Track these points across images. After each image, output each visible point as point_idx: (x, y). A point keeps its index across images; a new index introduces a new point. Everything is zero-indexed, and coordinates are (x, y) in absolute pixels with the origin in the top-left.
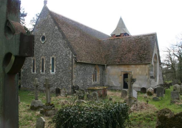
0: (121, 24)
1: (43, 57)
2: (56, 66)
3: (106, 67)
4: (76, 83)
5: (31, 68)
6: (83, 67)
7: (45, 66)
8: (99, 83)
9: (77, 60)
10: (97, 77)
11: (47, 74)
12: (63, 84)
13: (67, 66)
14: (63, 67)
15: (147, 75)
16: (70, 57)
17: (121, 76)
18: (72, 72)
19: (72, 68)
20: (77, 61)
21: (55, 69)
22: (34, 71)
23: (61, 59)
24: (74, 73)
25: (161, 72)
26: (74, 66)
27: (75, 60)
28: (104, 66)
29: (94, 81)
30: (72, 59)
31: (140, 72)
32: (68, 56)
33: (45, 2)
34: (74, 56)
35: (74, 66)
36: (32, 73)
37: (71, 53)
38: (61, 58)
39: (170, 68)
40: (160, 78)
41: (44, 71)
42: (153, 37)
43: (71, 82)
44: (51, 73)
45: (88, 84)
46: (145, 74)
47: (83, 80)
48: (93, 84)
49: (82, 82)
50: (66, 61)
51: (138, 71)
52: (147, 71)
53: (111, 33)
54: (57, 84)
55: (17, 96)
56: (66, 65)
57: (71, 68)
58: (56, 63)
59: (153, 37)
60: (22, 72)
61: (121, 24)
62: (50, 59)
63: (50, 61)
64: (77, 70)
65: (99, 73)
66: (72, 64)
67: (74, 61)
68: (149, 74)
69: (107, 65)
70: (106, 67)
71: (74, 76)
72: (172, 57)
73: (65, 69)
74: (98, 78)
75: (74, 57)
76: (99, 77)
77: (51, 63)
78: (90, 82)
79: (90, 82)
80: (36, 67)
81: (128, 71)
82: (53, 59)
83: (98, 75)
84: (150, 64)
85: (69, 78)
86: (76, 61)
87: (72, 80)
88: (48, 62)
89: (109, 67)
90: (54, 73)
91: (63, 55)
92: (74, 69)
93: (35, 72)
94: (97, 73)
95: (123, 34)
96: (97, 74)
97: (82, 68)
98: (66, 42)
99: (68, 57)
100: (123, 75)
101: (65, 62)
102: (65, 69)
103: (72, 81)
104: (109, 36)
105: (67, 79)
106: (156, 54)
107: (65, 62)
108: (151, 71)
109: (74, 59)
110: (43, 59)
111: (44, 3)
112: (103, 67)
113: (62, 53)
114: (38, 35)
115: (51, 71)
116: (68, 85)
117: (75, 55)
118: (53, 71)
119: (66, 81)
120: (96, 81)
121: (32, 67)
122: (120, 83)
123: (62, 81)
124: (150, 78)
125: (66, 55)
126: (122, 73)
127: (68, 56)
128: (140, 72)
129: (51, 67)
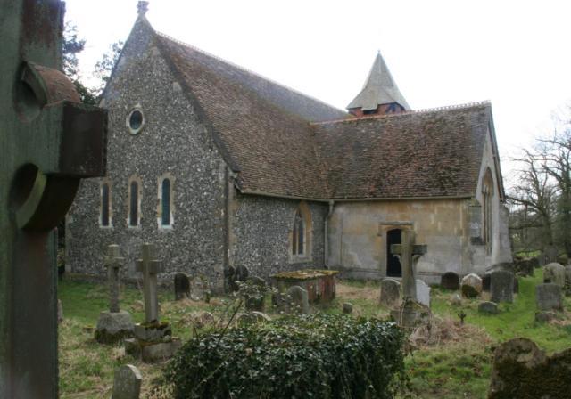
0: (380, 75)
1: (134, 178)
2: (177, 205)
3: (331, 208)
4: (239, 258)
5: (97, 213)
6: (261, 209)
7: (142, 205)
8: (311, 259)
9: (242, 188)
10: (305, 240)
11: (148, 230)
12: (196, 262)
13: (210, 207)
14: (198, 209)
15: (460, 233)
16: (221, 177)
17: (380, 238)
18: (226, 225)
19: (226, 213)
20: (242, 191)
21: (171, 214)
22: (105, 222)
23: (192, 185)
24: (231, 226)
25: (504, 225)
26: (233, 206)
27: (235, 187)
28: (326, 204)
29: (294, 253)
30: (227, 185)
31: (439, 224)
32: (214, 173)
33: (142, 7)
34: (231, 173)
35: (233, 206)
36: (101, 227)
37: (223, 164)
38: (190, 182)
39: (533, 213)
40: (503, 242)
41: (139, 223)
42: (481, 114)
43: (223, 255)
44: (161, 227)
45: (277, 263)
46: (455, 230)
47: (262, 250)
48: (290, 262)
49: (257, 255)
50: (207, 191)
51: (433, 222)
52: (461, 222)
53: (347, 104)
54: (180, 262)
55: (52, 298)
56: (208, 204)
57: (223, 213)
58: (176, 196)
59: (481, 114)
60: (70, 224)
61: (380, 75)
62: (156, 185)
63: (156, 190)
64: (240, 219)
65: (311, 229)
66: (226, 201)
67: (231, 191)
68: (468, 230)
69: (336, 204)
70: (333, 210)
71: (232, 236)
72: (539, 178)
73: (205, 215)
74: (308, 242)
75: (232, 177)
76: (311, 239)
77: (160, 196)
78: (283, 255)
79: (283, 255)
80: (114, 208)
81: (401, 222)
82: (166, 183)
83: (308, 234)
84: (469, 198)
85: (216, 243)
86: (238, 191)
87: (226, 248)
88: (150, 193)
89: (341, 210)
90: (169, 227)
91: (199, 170)
92: (231, 216)
93: (111, 225)
94: (305, 226)
95: (386, 107)
96: (305, 232)
97: (257, 213)
98: (206, 131)
99: (213, 179)
100: (385, 235)
101: (205, 194)
102: (205, 215)
103: (226, 253)
104: (341, 113)
105: (210, 247)
106: (488, 168)
107: (205, 194)
108: (474, 222)
109: (231, 185)
110: (135, 185)
111: (137, 9)
112: (324, 207)
113: (194, 166)
114: (118, 109)
115: (159, 221)
116: (212, 264)
117: (235, 172)
118: (166, 222)
119: (208, 252)
120: (301, 252)
121: (100, 210)
122: (376, 258)
123: (194, 252)
124: (469, 243)
125: (208, 172)
126: (384, 227)
127: (214, 173)
128: (439, 224)
129: (159, 209)
